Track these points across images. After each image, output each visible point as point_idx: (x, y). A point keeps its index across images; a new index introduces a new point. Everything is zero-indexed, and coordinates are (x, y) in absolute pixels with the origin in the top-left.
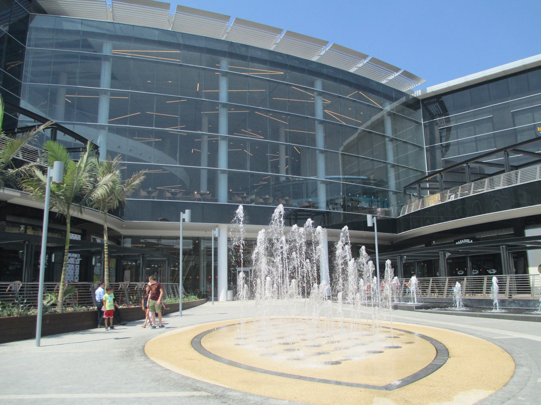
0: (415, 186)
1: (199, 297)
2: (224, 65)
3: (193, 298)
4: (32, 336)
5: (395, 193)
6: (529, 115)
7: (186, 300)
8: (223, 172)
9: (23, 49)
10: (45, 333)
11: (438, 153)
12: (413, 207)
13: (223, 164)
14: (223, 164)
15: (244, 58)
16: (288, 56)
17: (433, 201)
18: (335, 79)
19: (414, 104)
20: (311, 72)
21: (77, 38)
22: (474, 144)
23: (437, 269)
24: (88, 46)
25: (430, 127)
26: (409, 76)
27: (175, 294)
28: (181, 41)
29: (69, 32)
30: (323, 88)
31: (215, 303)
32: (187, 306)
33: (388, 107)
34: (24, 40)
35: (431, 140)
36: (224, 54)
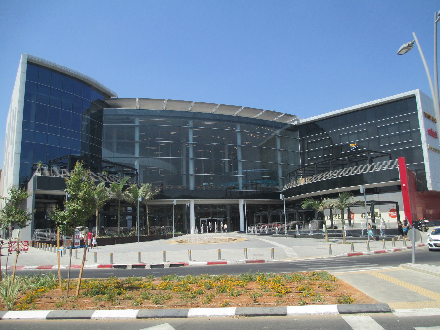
0: (294, 174)
1: (182, 232)
2: (191, 123)
3: (179, 233)
4: (137, 242)
5: (281, 178)
6: (347, 137)
7: (176, 233)
8: (192, 175)
9: (102, 126)
10: (140, 241)
11: (306, 155)
12: (292, 185)
13: (191, 172)
14: (191, 172)
15: (200, 119)
16: (222, 115)
17: (302, 182)
18: (247, 123)
19: (294, 128)
20: (233, 121)
21: (125, 117)
22: (323, 151)
23: (314, 217)
24: (128, 119)
25: (302, 141)
26: (288, 116)
27: (172, 231)
28: (170, 115)
29: (120, 115)
30: (241, 128)
31: (189, 235)
32: (176, 236)
33: (278, 132)
34: (102, 122)
35: (302, 149)
36: (190, 118)
